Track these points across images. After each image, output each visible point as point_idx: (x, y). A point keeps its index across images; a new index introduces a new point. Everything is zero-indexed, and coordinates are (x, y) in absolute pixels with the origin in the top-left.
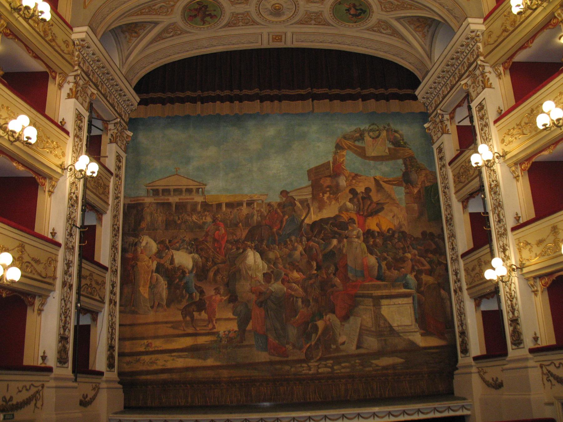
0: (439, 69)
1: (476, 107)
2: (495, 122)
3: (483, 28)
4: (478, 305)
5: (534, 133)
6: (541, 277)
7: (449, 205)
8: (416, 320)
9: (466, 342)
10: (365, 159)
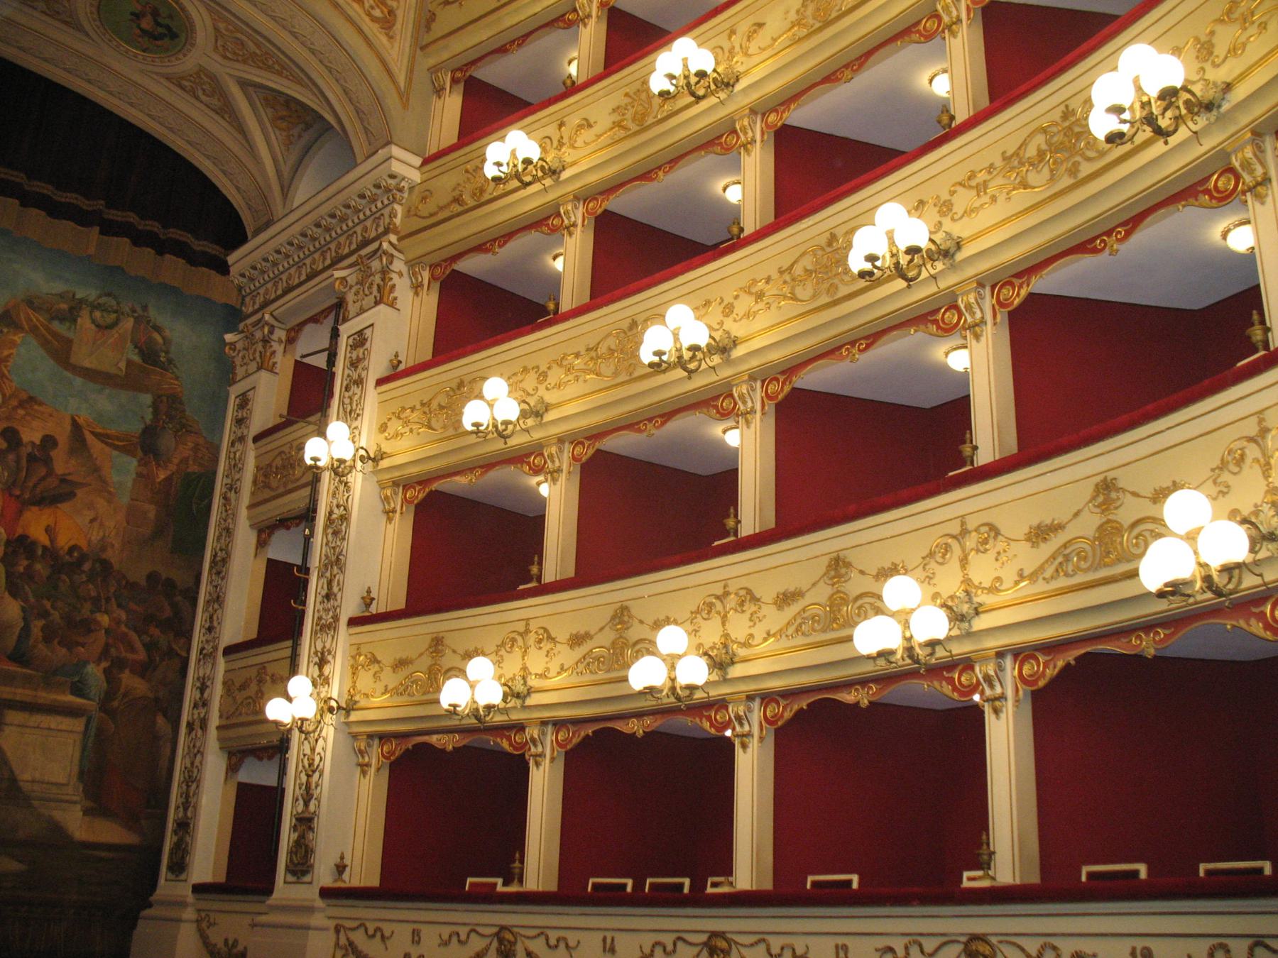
0: (297, 228)
1: (348, 337)
2: (380, 382)
3: (416, 176)
4: (232, 769)
5: (451, 432)
6: (383, 738)
7: (228, 530)
8: (81, 774)
9: (187, 845)
10: (66, 369)
